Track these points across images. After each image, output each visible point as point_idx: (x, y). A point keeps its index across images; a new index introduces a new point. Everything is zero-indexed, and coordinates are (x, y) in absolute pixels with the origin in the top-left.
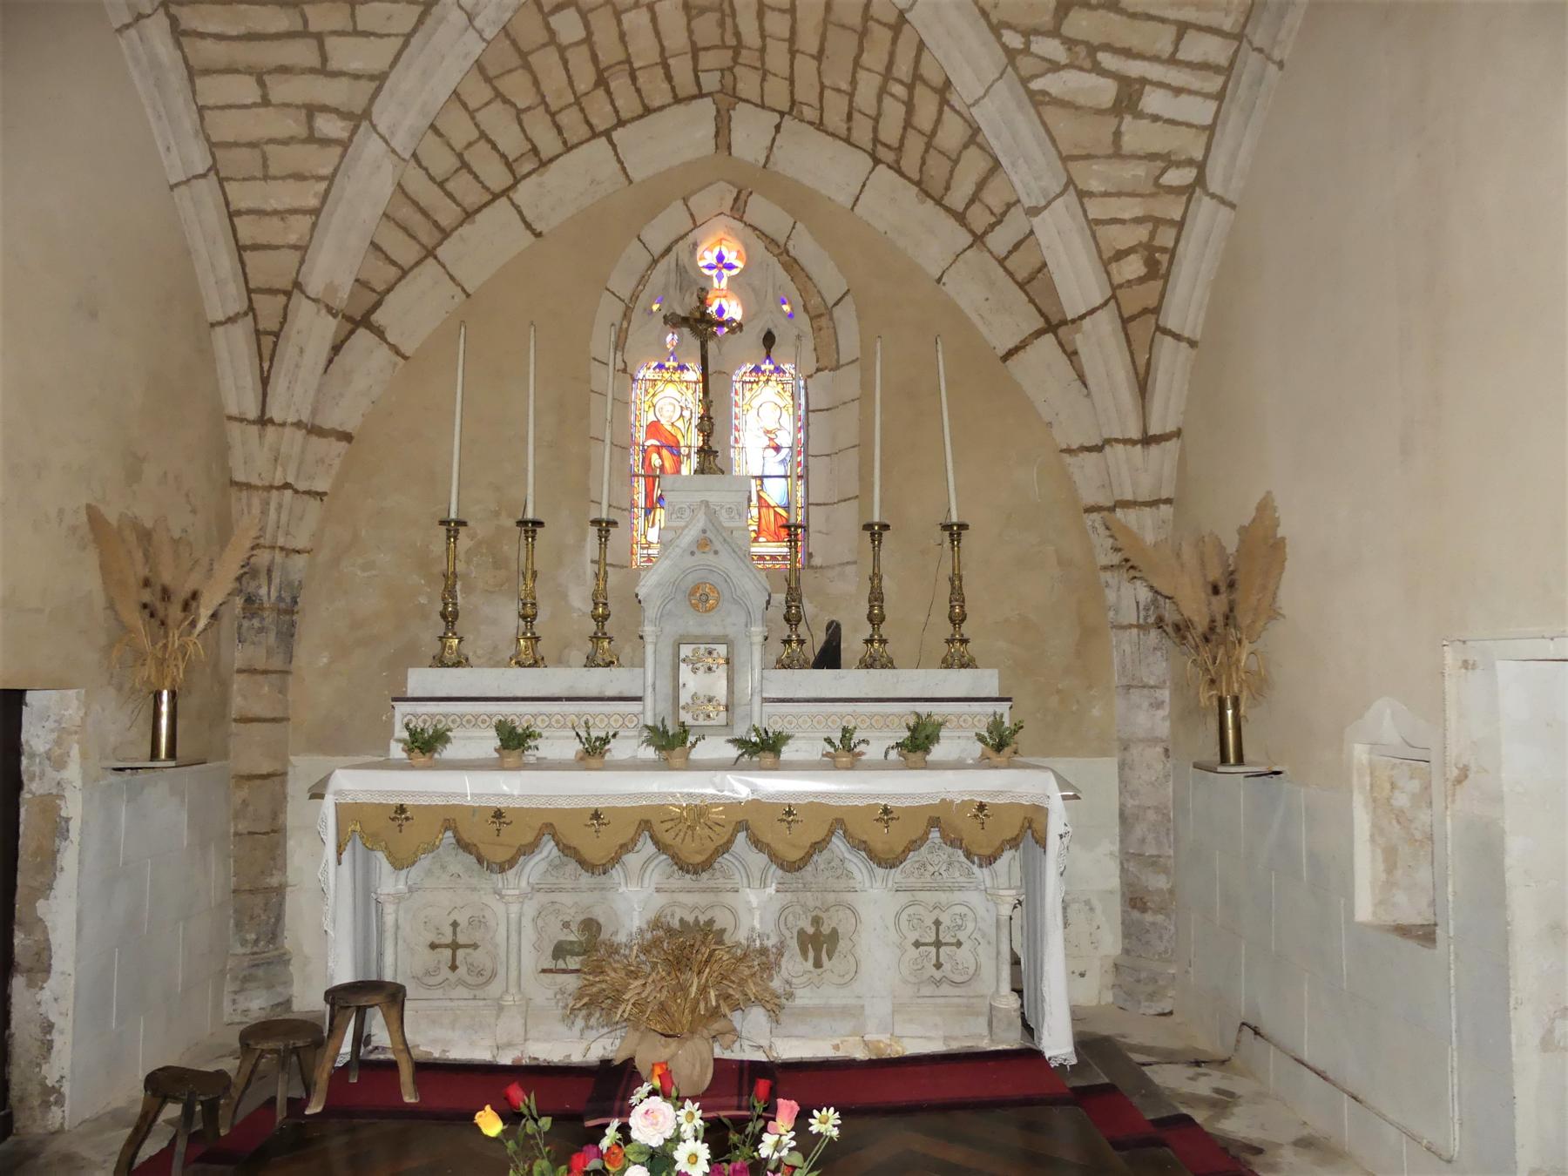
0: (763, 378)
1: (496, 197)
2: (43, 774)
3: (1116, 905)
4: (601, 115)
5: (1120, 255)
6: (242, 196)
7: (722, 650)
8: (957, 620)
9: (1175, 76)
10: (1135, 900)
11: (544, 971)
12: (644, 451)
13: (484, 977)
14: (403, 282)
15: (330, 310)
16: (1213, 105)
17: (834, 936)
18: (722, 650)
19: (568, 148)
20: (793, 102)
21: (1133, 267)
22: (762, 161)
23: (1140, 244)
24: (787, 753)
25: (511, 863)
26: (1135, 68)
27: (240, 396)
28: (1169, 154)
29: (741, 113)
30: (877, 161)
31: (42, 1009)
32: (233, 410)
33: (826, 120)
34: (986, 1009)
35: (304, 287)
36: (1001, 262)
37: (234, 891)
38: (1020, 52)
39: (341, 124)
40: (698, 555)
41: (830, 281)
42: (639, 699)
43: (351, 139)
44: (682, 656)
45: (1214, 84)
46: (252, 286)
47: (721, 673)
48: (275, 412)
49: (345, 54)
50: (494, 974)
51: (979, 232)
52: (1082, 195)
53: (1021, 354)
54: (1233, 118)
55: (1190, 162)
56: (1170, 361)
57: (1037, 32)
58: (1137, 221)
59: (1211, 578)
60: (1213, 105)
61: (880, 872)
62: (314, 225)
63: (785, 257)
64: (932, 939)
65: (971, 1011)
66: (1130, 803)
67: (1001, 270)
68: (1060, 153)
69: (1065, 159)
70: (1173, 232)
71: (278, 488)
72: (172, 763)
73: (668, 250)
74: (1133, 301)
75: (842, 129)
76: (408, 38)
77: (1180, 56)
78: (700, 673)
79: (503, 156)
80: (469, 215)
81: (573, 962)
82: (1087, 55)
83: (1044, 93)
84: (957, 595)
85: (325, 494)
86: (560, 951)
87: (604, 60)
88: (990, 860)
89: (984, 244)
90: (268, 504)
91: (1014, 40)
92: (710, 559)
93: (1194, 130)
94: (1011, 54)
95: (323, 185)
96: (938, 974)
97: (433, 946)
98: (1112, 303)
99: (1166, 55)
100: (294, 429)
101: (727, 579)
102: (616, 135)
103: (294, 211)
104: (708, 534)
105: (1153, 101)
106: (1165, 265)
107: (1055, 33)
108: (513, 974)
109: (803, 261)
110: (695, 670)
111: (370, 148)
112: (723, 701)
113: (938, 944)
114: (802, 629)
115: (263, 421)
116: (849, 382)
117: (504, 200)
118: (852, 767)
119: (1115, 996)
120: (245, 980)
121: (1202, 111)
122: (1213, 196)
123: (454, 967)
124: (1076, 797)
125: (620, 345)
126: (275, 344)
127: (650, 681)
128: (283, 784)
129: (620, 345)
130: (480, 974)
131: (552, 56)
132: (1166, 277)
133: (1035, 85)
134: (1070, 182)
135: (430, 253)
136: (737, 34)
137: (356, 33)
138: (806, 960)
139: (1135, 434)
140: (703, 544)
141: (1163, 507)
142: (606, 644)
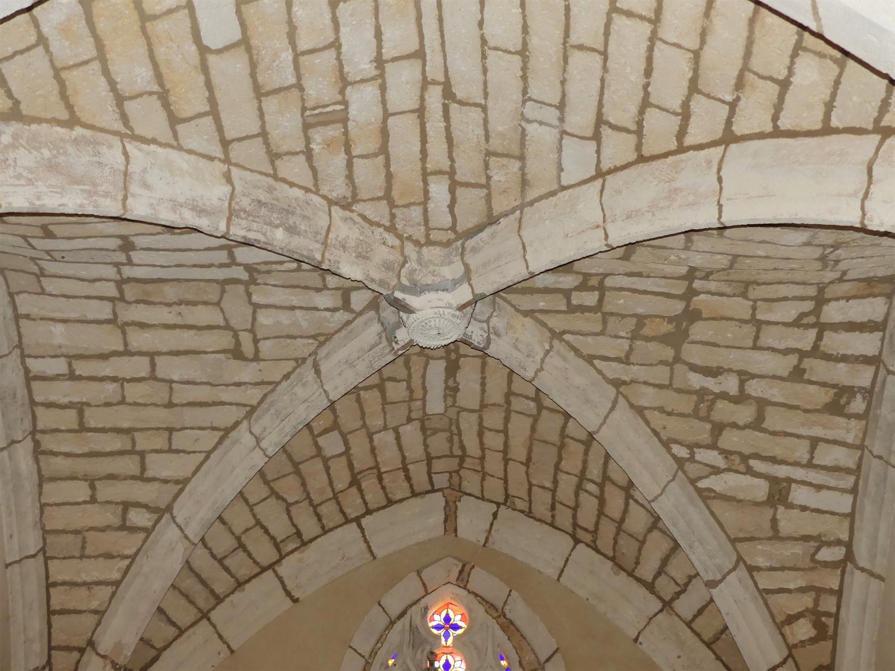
1: (264, 570)
4: (353, 504)
5: (791, 619)
6: (60, 571)
19: (325, 531)
20: (507, 496)
21: (803, 630)
22: (482, 541)
23: (807, 610)
26: (782, 471)
28: (819, 536)
29: (466, 506)
30: (577, 541)
36: (689, 624)
38: (688, 460)
39: (147, 515)
43: (154, 527)
45: (848, 481)
49: (160, 466)
51: (667, 598)
52: (752, 569)
54: (868, 509)
55: (839, 542)
57: (699, 446)
58: (802, 590)
62: (114, 594)
63: (502, 620)
67: (689, 631)
69: (734, 541)
79: (273, 538)
80: (240, 584)
91: (681, 452)
95: (127, 562)
98: (790, 661)
99: (805, 461)
102: (364, 522)
105: (799, 495)
107: (713, 446)
109: (518, 623)
111: (168, 534)
121: (844, 503)
122: (863, 570)
131: (319, 465)
133: (702, 484)
134: (740, 559)
135: (205, 615)
136: (463, 448)
137: (171, 451)
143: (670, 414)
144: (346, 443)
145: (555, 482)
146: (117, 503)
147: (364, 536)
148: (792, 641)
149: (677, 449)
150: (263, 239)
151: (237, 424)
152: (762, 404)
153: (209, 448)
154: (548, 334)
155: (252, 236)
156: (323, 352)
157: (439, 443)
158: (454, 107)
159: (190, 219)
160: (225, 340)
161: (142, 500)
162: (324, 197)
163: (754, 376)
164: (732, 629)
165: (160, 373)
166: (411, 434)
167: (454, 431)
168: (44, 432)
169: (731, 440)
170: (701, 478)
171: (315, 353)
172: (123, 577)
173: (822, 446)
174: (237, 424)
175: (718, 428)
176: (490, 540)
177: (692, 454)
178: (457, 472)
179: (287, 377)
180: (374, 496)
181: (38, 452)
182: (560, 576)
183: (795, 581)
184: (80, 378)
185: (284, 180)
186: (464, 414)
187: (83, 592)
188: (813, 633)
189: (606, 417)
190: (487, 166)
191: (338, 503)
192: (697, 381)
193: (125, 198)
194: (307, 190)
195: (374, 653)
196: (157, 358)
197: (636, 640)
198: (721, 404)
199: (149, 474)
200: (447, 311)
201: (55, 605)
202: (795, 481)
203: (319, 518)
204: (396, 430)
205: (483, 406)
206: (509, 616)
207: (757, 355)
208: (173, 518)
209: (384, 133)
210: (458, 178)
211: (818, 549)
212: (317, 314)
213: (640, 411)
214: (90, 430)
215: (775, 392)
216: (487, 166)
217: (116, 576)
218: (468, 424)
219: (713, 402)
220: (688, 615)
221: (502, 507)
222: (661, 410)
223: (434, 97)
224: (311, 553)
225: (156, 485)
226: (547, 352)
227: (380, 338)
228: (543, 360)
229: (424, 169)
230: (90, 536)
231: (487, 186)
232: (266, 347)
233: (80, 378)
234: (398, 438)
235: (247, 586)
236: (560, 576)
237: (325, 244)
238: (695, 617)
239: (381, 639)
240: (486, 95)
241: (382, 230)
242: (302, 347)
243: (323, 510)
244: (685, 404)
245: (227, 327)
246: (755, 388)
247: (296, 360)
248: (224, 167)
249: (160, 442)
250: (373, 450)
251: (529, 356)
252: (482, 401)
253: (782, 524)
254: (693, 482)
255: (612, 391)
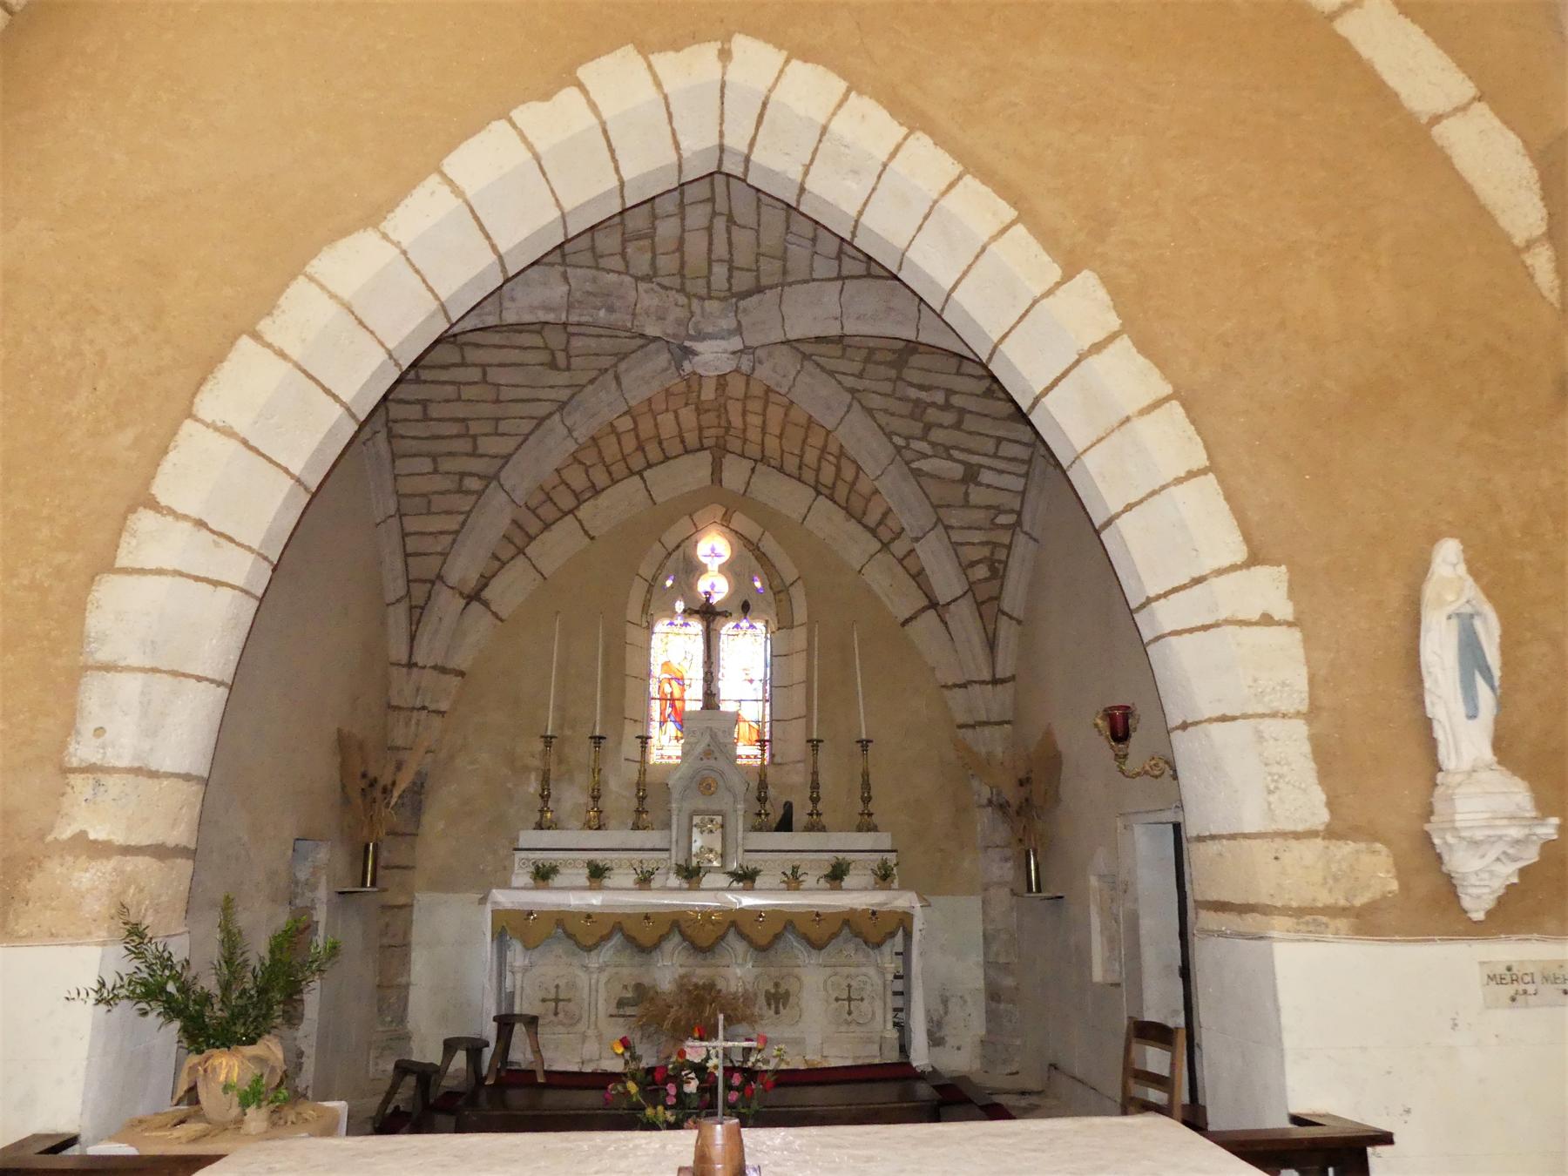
0: (742, 632)
1: (566, 514)
2: (303, 894)
3: (982, 997)
4: (637, 462)
5: (973, 564)
6: (412, 524)
7: (719, 819)
8: (867, 800)
9: (1001, 465)
10: (994, 995)
11: (611, 1016)
12: (660, 682)
13: (574, 1020)
14: (502, 571)
15: (461, 594)
16: (1023, 481)
17: (787, 994)
18: (719, 819)
19: (614, 482)
20: (763, 456)
21: (981, 572)
22: (742, 492)
23: (985, 558)
24: (759, 882)
25: (596, 946)
26: (975, 459)
27: (399, 651)
28: (998, 506)
29: (729, 461)
30: (819, 493)
31: (297, 1043)
32: (393, 659)
33: (784, 467)
34: (877, 1039)
35: (445, 579)
36: (901, 561)
37: (379, 986)
38: (904, 447)
39: (479, 482)
40: (705, 761)
41: (789, 572)
42: (667, 850)
43: (484, 491)
44: (694, 823)
45: (1023, 469)
46: (410, 578)
47: (718, 833)
48: (419, 658)
49: (489, 445)
50: (579, 1020)
51: (885, 541)
52: (947, 528)
53: (914, 623)
54: (1032, 494)
55: (1012, 511)
56: (1006, 629)
57: (913, 438)
58: (983, 544)
59: (1020, 777)
60: (1023, 481)
61: (813, 951)
62: (454, 541)
63: (757, 552)
64: (845, 997)
65: (870, 1041)
66: (989, 927)
67: (900, 567)
68: (931, 503)
69: (935, 507)
70: (1005, 551)
71: (419, 709)
72: (375, 889)
73: (678, 546)
74: (983, 592)
75: (796, 472)
76: (527, 437)
77: (1000, 453)
78: (705, 833)
79: (573, 491)
80: (547, 526)
81: (629, 1011)
82: (946, 451)
83: (920, 470)
84: (866, 785)
85: (445, 712)
86: (621, 1003)
87: (643, 436)
88: (878, 945)
89: (889, 549)
90: (410, 720)
91: (900, 442)
92: (712, 762)
93: (1012, 494)
94: (898, 449)
95: (462, 517)
96: (849, 1018)
97: (544, 1000)
98: (970, 593)
99: (991, 453)
100: (430, 670)
101: (722, 774)
102: (645, 474)
103: (441, 533)
104: (712, 748)
105: (986, 477)
106: (1001, 571)
107: (923, 438)
108: (593, 1018)
109: (769, 555)
110: (702, 832)
111: (496, 499)
112: (719, 851)
113: (850, 999)
114: (768, 806)
115: (411, 665)
116: (800, 636)
117: (570, 517)
118: (797, 889)
119: (982, 1064)
120: (384, 1049)
121: (1017, 484)
122: (1026, 533)
123: (556, 1014)
124: (929, 906)
125: (645, 608)
126: (421, 614)
127: (674, 839)
128: (411, 912)
129: (645, 608)
130: (572, 1018)
131: (613, 439)
132: (1003, 577)
133: (915, 465)
134: (939, 519)
135: (521, 551)
136: (729, 422)
137: (497, 434)
138: (770, 1008)
139: (986, 676)
140: (708, 753)
141: (1006, 726)
142: (549, 815)
143: (893, 414)
144: (635, 422)
145: (802, 450)
146: (455, 474)
147: (646, 486)
148: (972, 579)
149: (897, 440)
150: (591, 320)
151: (551, 414)
152: (962, 412)
153: (526, 432)
154: (800, 356)
155: (584, 319)
156: (623, 366)
157: (709, 418)
158: (734, 228)
159: (543, 316)
160: (544, 357)
161: (474, 470)
162: (632, 276)
163: (956, 393)
164: (928, 571)
165: (489, 379)
166: (688, 416)
167: (722, 410)
168: (395, 421)
169: (937, 435)
170: (913, 461)
171: (615, 365)
172: (462, 528)
173: (1004, 443)
174: (551, 414)
175: (928, 427)
176: (749, 490)
177: (908, 444)
178: (723, 437)
179: (592, 381)
180: (653, 453)
181: (391, 436)
182: (804, 519)
183: (977, 537)
184: (425, 382)
185: (603, 269)
186: (731, 401)
187: (430, 539)
188: (988, 574)
189: (842, 419)
190: (757, 261)
191: (626, 463)
192: (913, 393)
193: (501, 311)
194: (619, 273)
195: (655, 578)
196: (488, 369)
197: (860, 571)
198: (930, 411)
199: (480, 451)
200: (724, 355)
201: (409, 549)
202: (985, 467)
203: (610, 474)
204: (676, 412)
205: (746, 397)
206: (762, 550)
207: (959, 379)
208: (502, 486)
209: (681, 241)
210: (735, 264)
211: (996, 516)
212: (619, 340)
213: (870, 412)
214: (431, 420)
215: (972, 404)
216: (757, 261)
217: (455, 527)
218: (734, 410)
219: (925, 408)
220: (900, 554)
221: (759, 464)
222: (886, 411)
223: (720, 224)
224: (603, 500)
225: (486, 459)
226: (799, 372)
227: (670, 364)
228: (795, 379)
229: (709, 258)
230: (434, 498)
231: (758, 270)
232: (575, 362)
233: (425, 382)
234: (677, 417)
235: (553, 527)
236: (804, 519)
237: (634, 315)
238: (905, 557)
239: (661, 566)
240: (759, 225)
241: (674, 292)
242: (606, 362)
243: (614, 468)
244: (905, 409)
245: (546, 348)
246: (956, 400)
247: (600, 370)
248: (561, 269)
249: (488, 428)
250: (656, 425)
251: (784, 376)
252: (746, 394)
253: (972, 497)
254: (907, 463)
255: (847, 397)
